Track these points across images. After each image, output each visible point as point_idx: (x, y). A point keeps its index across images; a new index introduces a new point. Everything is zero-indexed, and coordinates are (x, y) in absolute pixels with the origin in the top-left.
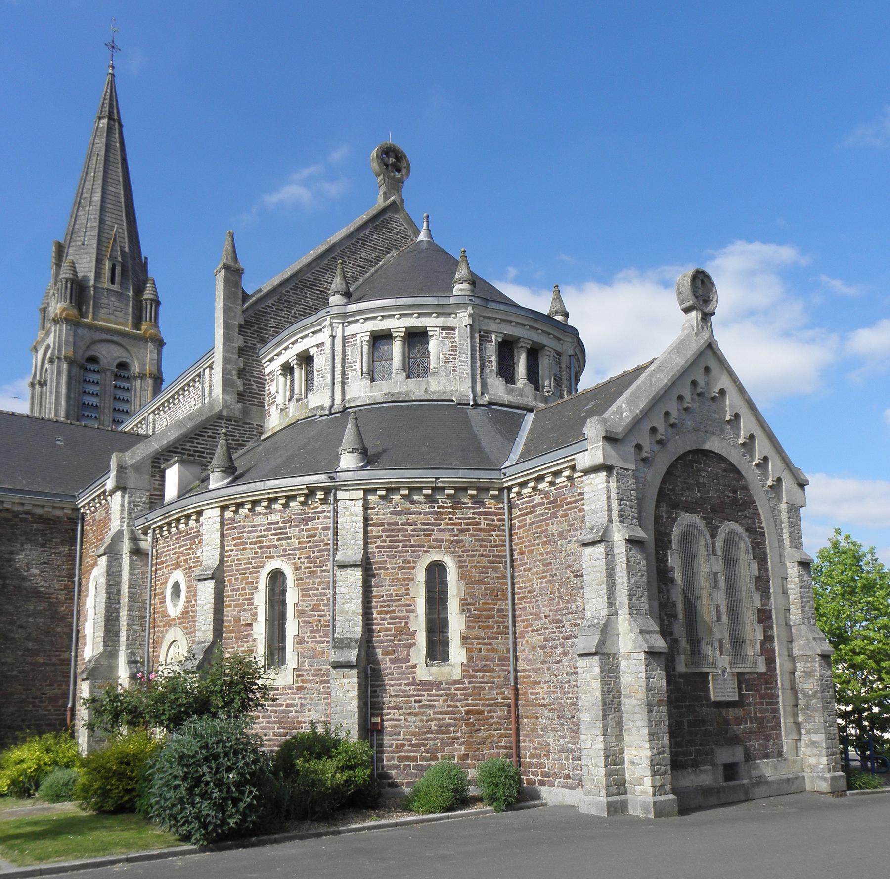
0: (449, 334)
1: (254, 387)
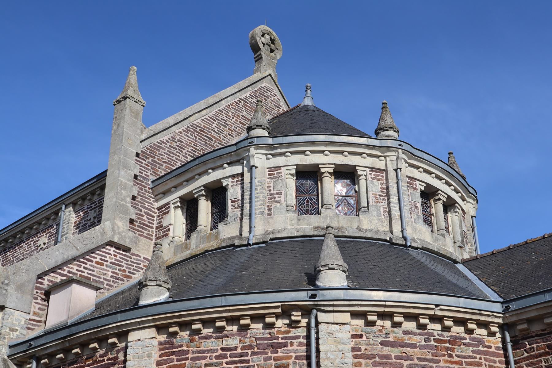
0: (378, 176)
1: (145, 218)
